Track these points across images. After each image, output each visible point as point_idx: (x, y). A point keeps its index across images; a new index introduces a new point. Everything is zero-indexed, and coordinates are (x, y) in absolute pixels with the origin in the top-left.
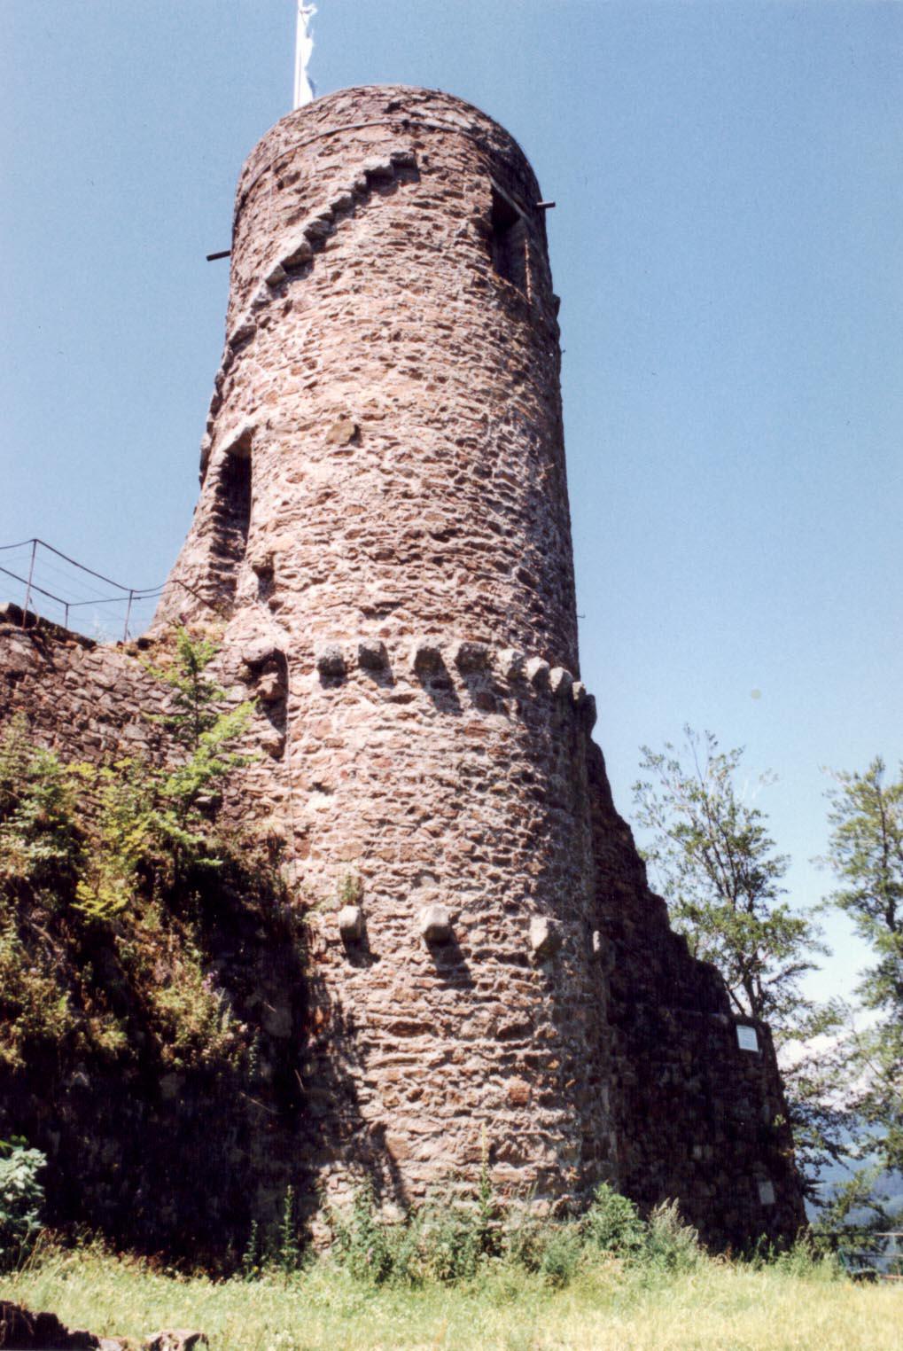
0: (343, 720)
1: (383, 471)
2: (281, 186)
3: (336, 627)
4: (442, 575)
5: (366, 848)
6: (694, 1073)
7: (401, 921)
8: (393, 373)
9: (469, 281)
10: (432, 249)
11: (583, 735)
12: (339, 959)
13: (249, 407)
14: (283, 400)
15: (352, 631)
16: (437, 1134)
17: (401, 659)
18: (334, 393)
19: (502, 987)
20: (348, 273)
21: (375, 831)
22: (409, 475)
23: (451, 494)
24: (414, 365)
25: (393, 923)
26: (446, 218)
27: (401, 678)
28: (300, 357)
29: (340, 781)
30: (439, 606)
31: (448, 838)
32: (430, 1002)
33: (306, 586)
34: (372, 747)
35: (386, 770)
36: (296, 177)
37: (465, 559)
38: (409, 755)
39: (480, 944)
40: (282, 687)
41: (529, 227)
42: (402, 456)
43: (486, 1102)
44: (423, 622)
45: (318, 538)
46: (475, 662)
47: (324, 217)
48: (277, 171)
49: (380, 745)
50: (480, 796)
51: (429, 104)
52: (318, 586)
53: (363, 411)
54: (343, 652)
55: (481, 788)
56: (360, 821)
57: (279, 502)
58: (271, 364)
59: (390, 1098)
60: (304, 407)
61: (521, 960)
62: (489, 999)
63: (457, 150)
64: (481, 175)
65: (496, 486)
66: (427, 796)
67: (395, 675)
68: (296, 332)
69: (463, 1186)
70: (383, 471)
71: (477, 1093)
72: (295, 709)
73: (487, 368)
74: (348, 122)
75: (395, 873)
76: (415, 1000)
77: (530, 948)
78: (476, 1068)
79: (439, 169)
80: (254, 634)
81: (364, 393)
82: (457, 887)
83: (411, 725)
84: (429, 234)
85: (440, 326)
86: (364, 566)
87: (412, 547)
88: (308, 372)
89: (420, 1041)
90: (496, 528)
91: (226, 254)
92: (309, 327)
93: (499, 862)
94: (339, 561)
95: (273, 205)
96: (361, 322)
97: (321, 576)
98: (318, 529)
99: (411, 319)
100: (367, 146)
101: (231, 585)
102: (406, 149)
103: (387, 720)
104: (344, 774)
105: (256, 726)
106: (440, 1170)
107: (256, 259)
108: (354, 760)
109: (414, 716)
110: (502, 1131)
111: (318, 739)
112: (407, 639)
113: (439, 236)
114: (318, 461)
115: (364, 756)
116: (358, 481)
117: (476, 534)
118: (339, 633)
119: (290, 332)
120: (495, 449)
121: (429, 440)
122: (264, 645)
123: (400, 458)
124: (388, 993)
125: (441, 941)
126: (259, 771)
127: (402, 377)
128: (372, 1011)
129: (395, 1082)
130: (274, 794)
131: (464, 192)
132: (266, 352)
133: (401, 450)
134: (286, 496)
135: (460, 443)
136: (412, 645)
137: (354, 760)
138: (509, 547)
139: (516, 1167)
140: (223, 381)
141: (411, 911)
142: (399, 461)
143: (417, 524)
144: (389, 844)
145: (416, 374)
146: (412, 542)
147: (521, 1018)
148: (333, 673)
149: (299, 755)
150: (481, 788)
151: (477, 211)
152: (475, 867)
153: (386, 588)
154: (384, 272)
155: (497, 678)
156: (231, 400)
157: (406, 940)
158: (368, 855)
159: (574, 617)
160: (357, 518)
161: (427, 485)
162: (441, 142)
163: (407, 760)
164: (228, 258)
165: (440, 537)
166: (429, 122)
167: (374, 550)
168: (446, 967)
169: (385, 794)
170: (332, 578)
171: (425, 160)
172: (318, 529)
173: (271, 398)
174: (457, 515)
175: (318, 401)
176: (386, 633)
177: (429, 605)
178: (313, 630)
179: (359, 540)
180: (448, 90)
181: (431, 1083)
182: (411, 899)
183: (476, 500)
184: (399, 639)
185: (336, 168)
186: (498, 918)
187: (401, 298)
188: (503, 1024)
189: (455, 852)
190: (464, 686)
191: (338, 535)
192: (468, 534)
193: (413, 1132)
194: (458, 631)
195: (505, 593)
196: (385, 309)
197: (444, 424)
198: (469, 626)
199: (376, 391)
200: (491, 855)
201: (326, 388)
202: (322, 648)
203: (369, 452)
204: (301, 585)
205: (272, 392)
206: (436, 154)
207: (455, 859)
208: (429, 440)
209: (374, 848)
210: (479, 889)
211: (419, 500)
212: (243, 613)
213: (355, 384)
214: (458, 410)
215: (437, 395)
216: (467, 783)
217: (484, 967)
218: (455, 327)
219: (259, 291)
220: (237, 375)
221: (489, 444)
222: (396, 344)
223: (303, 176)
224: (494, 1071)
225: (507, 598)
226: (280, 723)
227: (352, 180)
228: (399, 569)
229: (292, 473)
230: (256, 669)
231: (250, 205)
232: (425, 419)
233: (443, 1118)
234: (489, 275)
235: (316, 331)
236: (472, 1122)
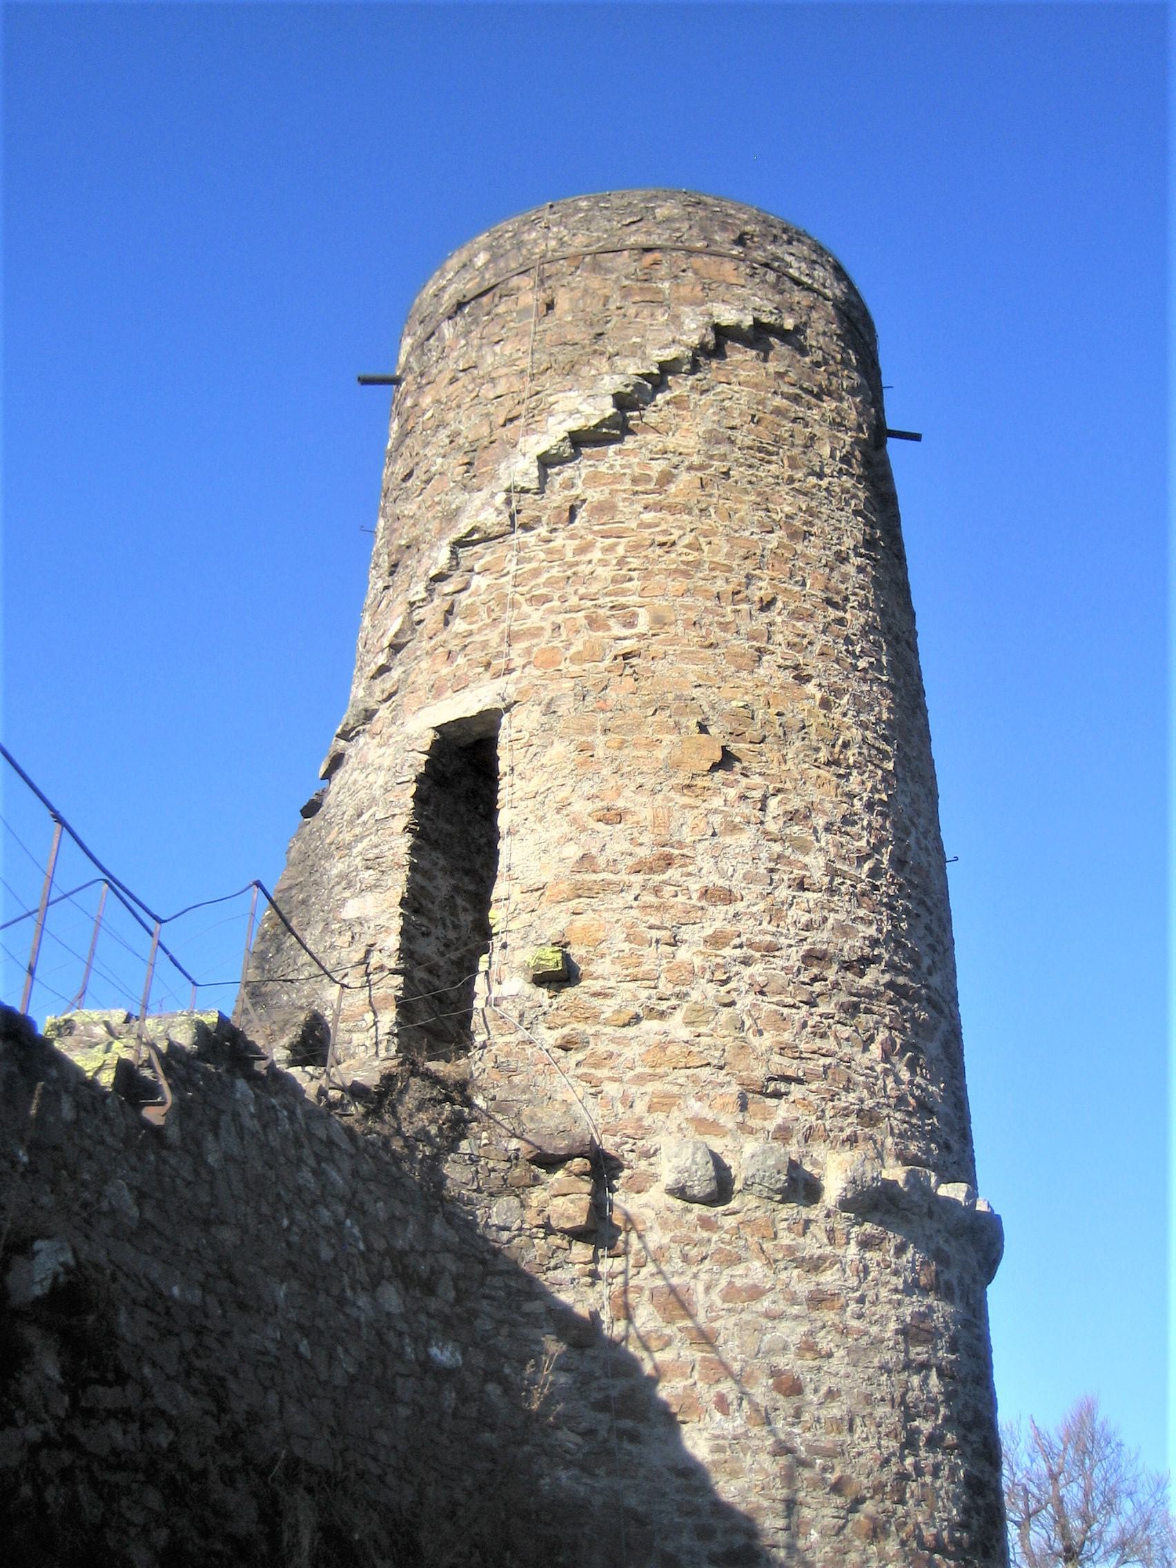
33: (637, 1019)
45: (655, 934)
58: (546, 599)
68: (596, 555)
97: (664, 1006)
178: (650, 1109)
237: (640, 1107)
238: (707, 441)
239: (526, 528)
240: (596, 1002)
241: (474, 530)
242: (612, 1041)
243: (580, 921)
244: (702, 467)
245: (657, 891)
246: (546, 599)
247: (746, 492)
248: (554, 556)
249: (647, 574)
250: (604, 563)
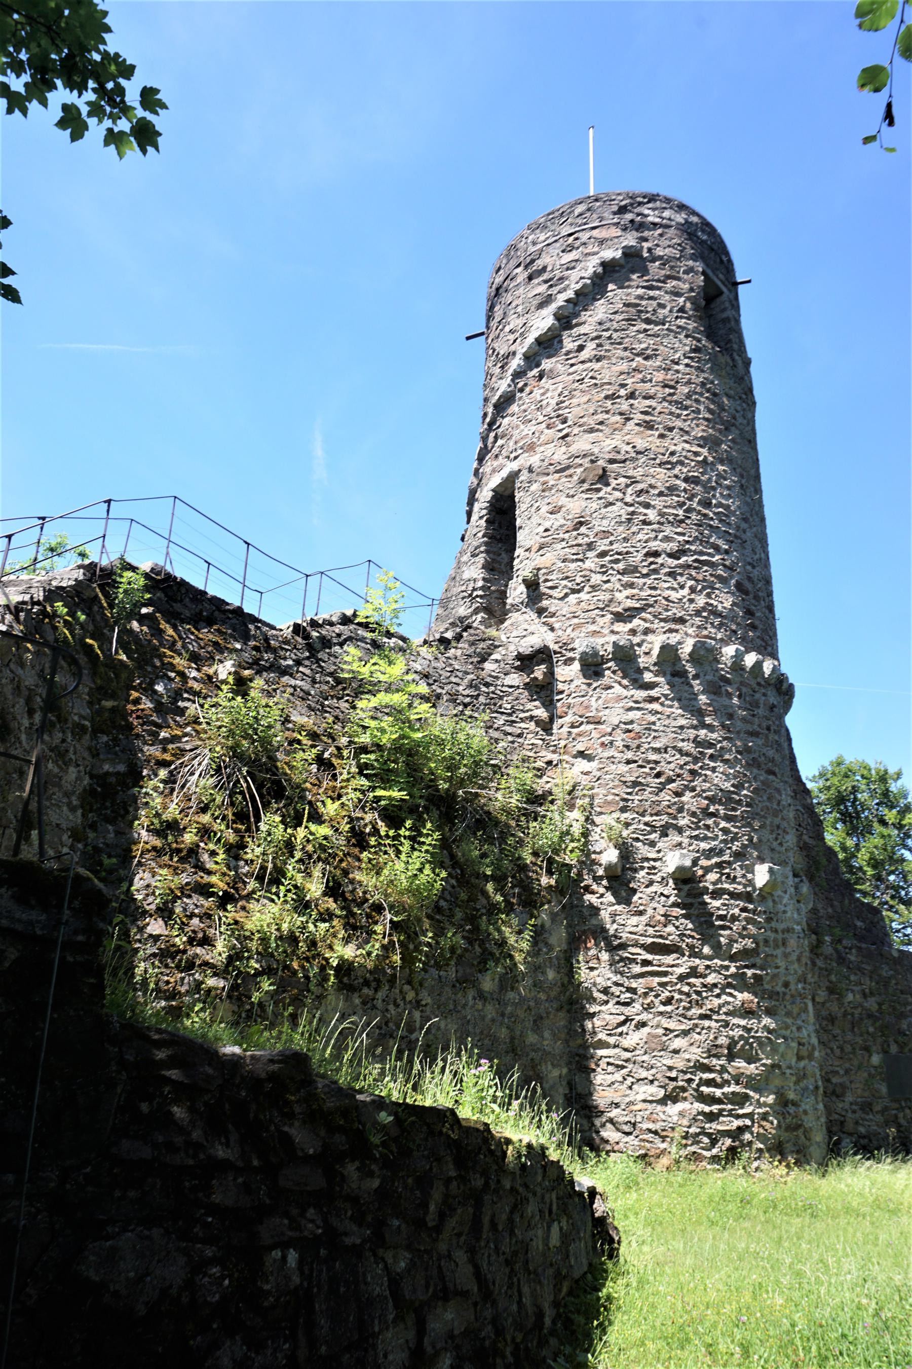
0: (600, 702)
1: (626, 504)
2: (530, 278)
3: (593, 628)
4: (676, 586)
5: (622, 804)
7: (652, 863)
8: (630, 425)
9: (688, 348)
10: (656, 324)
12: (602, 890)
13: (512, 456)
14: (542, 449)
15: (606, 631)
16: (685, 1033)
17: (646, 654)
18: (582, 443)
19: (734, 918)
20: (591, 345)
21: (630, 790)
22: (647, 506)
23: (682, 521)
24: (648, 418)
25: (646, 864)
26: (667, 297)
27: (647, 669)
29: (600, 750)
30: (674, 610)
31: (687, 797)
32: (677, 928)
33: (566, 595)
34: (625, 723)
35: (637, 742)
36: (544, 269)
37: (693, 573)
38: (655, 731)
39: (714, 884)
40: (550, 673)
42: (641, 491)
43: (724, 1010)
44: (662, 624)
45: (575, 557)
46: (704, 655)
47: (568, 301)
48: (526, 267)
49: (632, 722)
50: (712, 764)
51: (650, 205)
52: (576, 595)
53: (608, 456)
54: (599, 647)
55: (712, 757)
56: (617, 783)
57: (541, 529)
59: (647, 1001)
60: (560, 455)
61: (748, 897)
63: (674, 241)
64: (695, 261)
65: (715, 513)
66: (671, 764)
67: (642, 665)
68: (549, 395)
69: (706, 1076)
70: (626, 504)
71: (716, 1002)
72: (562, 692)
73: (704, 419)
74: (585, 224)
75: (646, 824)
76: (665, 926)
77: (755, 889)
78: (716, 981)
79: (660, 258)
80: (525, 633)
81: (608, 441)
82: (696, 838)
83: (656, 706)
85: (666, 386)
86: (613, 579)
87: (652, 563)
88: (561, 427)
89: (669, 959)
90: (717, 548)
91: (482, 334)
92: (560, 390)
93: (728, 818)
94: (593, 575)
95: (524, 293)
96: (603, 385)
98: (574, 550)
99: (643, 381)
100: (602, 242)
101: (503, 595)
102: (633, 243)
103: (636, 702)
104: (603, 744)
105: (529, 706)
106: (689, 1060)
107: (512, 337)
108: (610, 734)
109: (657, 699)
110: (737, 1033)
111: (581, 716)
112: (650, 638)
113: (662, 312)
114: (573, 496)
115: (618, 731)
116: (606, 515)
117: (701, 553)
118: (595, 633)
119: (544, 393)
120: (714, 484)
121: (661, 477)
122: (527, 645)
123: (640, 493)
124: (644, 919)
125: (685, 880)
126: (533, 741)
127: (637, 428)
128: (631, 933)
129: (651, 990)
130: (546, 760)
131: (681, 275)
132: (525, 411)
133: (639, 487)
134: (547, 524)
135: (686, 480)
136: (656, 642)
137: (610, 734)
138: (727, 563)
139: (749, 1063)
140: (488, 436)
141: (660, 855)
142: (638, 496)
143: (654, 545)
144: (641, 801)
145: (649, 426)
146: (651, 559)
147: (749, 943)
148: (592, 667)
149: (565, 729)
150: (712, 757)
151: (691, 290)
152: (710, 822)
153: (631, 597)
154: (620, 343)
155: (722, 669)
156: (495, 450)
157: (657, 878)
158: (624, 810)
160: (607, 541)
161: (662, 514)
162: (661, 235)
163: (653, 734)
164: (484, 337)
165: (671, 555)
166: (650, 219)
167: (621, 566)
168: (690, 900)
169: (635, 762)
170: (587, 589)
171: (650, 250)
172: (574, 550)
173: (531, 448)
174: (686, 538)
175: (571, 449)
176: (633, 632)
177: (667, 610)
179: (608, 558)
180: (664, 192)
181: (681, 992)
182: (660, 845)
183: (700, 526)
184: (643, 637)
185: (576, 261)
186: (729, 863)
187: (634, 364)
188: (736, 948)
189: (693, 809)
190: (696, 677)
192: (695, 553)
193: (666, 1029)
194: (690, 631)
195: (725, 601)
196: (622, 373)
197: (674, 465)
198: (699, 627)
199: (616, 441)
200: (722, 812)
201: (577, 438)
202: (581, 645)
203: (614, 489)
204: (562, 595)
205: (532, 443)
206: (657, 245)
207: (694, 814)
208: (661, 477)
209: (629, 803)
210: (714, 839)
211: (655, 526)
212: (514, 617)
213: (601, 434)
214: (684, 454)
215: (666, 442)
216: (701, 753)
217: (717, 903)
218: (678, 386)
219: (516, 363)
220: (500, 430)
221: (710, 480)
222: (632, 401)
223: (549, 268)
224: (729, 985)
225: (728, 605)
226: (549, 704)
227: (591, 271)
228: (642, 581)
229: (551, 506)
230: (526, 662)
231: (504, 294)
232: (658, 461)
233: (690, 1019)
235: (566, 393)
236: (713, 1024)
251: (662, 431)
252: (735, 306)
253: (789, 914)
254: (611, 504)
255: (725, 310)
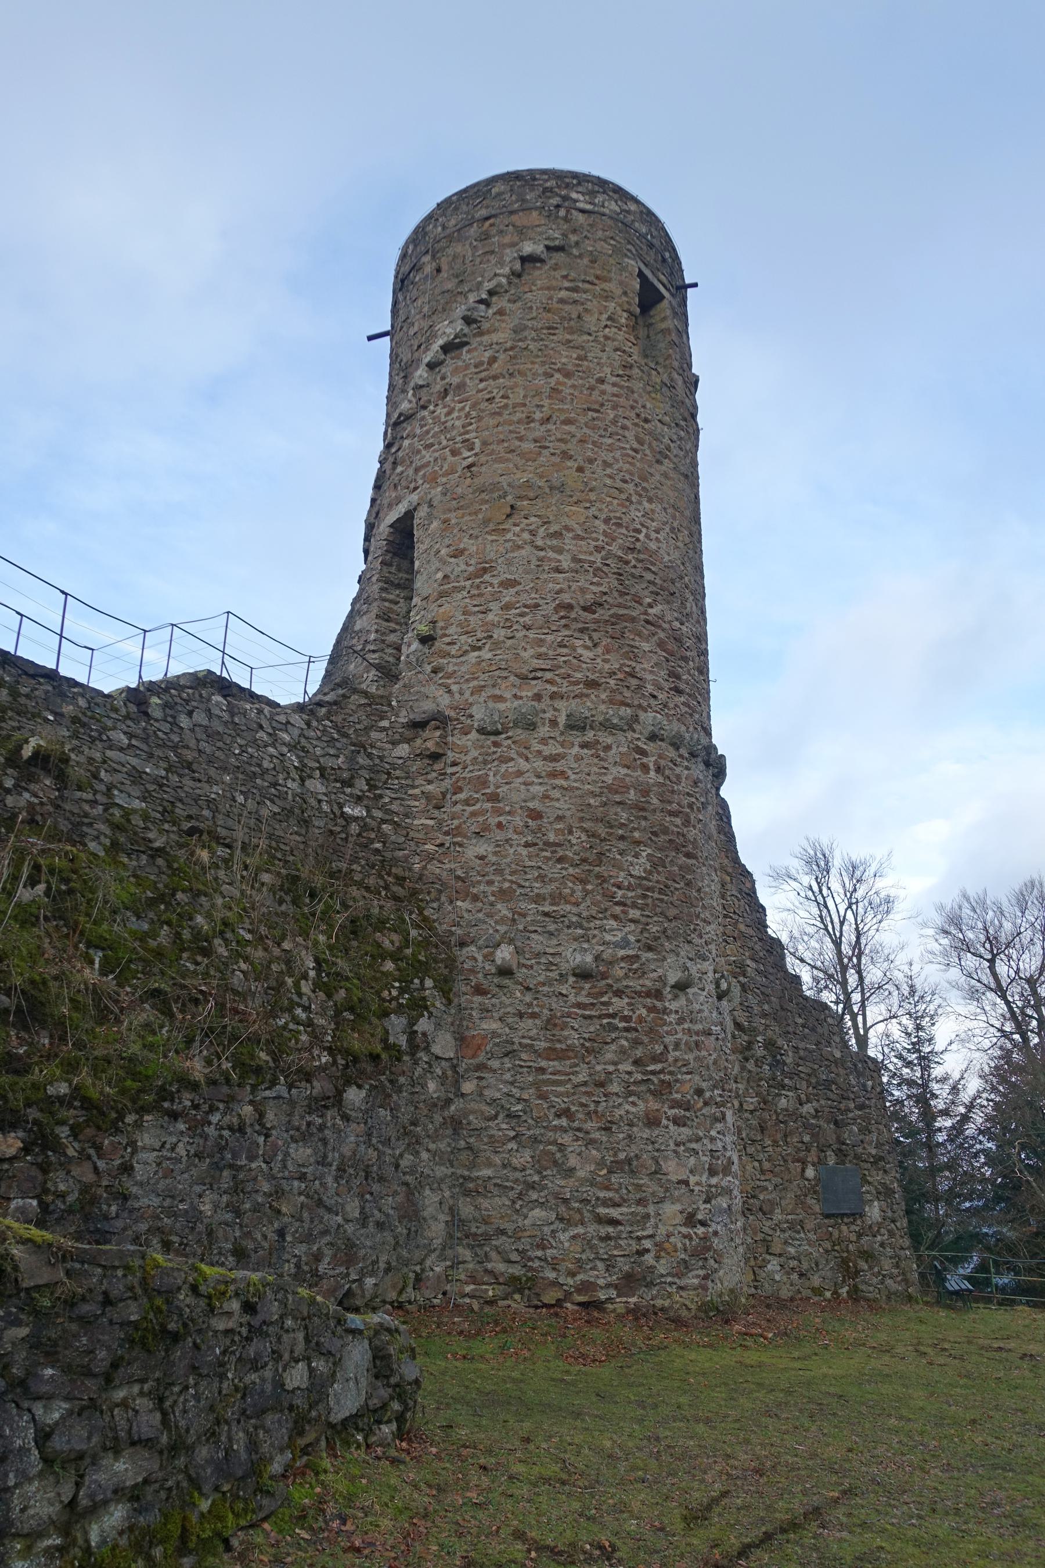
1: (537, 548)
6: (808, 1101)
11: (714, 791)
13: (412, 486)
22: (560, 551)
28: (459, 439)
33: (466, 652)
41: (673, 309)
45: (477, 609)
52: (476, 654)
57: (440, 575)
58: (432, 445)
62: (627, 1030)
68: (455, 414)
70: (537, 548)
84: (579, 317)
88: (466, 454)
97: (480, 644)
130: (438, 842)
143: (566, 598)
153: (539, 656)
159: (707, 681)
160: (513, 591)
161: (575, 560)
169: (536, 844)
174: (602, 589)
178: (472, 694)
191: (495, 606)
232: (575, 499)
234: (635, 357)
237: (467, 694)
238: (515, 332)
239: (424, 407)
240: (448, 648)
241: (400, 415)
242: (456, 664)
243: (442, 610)
244: (512, 348)
245: (478, 587)
246: (432, 445)
247: (538, 356)
248: (436, 420)
249: (480, 418)
250: (458, 418)
251: (582, 463)
252: (683, 316)
253: (706, 1014)
254: (519, 547)
255: (664, 319)
